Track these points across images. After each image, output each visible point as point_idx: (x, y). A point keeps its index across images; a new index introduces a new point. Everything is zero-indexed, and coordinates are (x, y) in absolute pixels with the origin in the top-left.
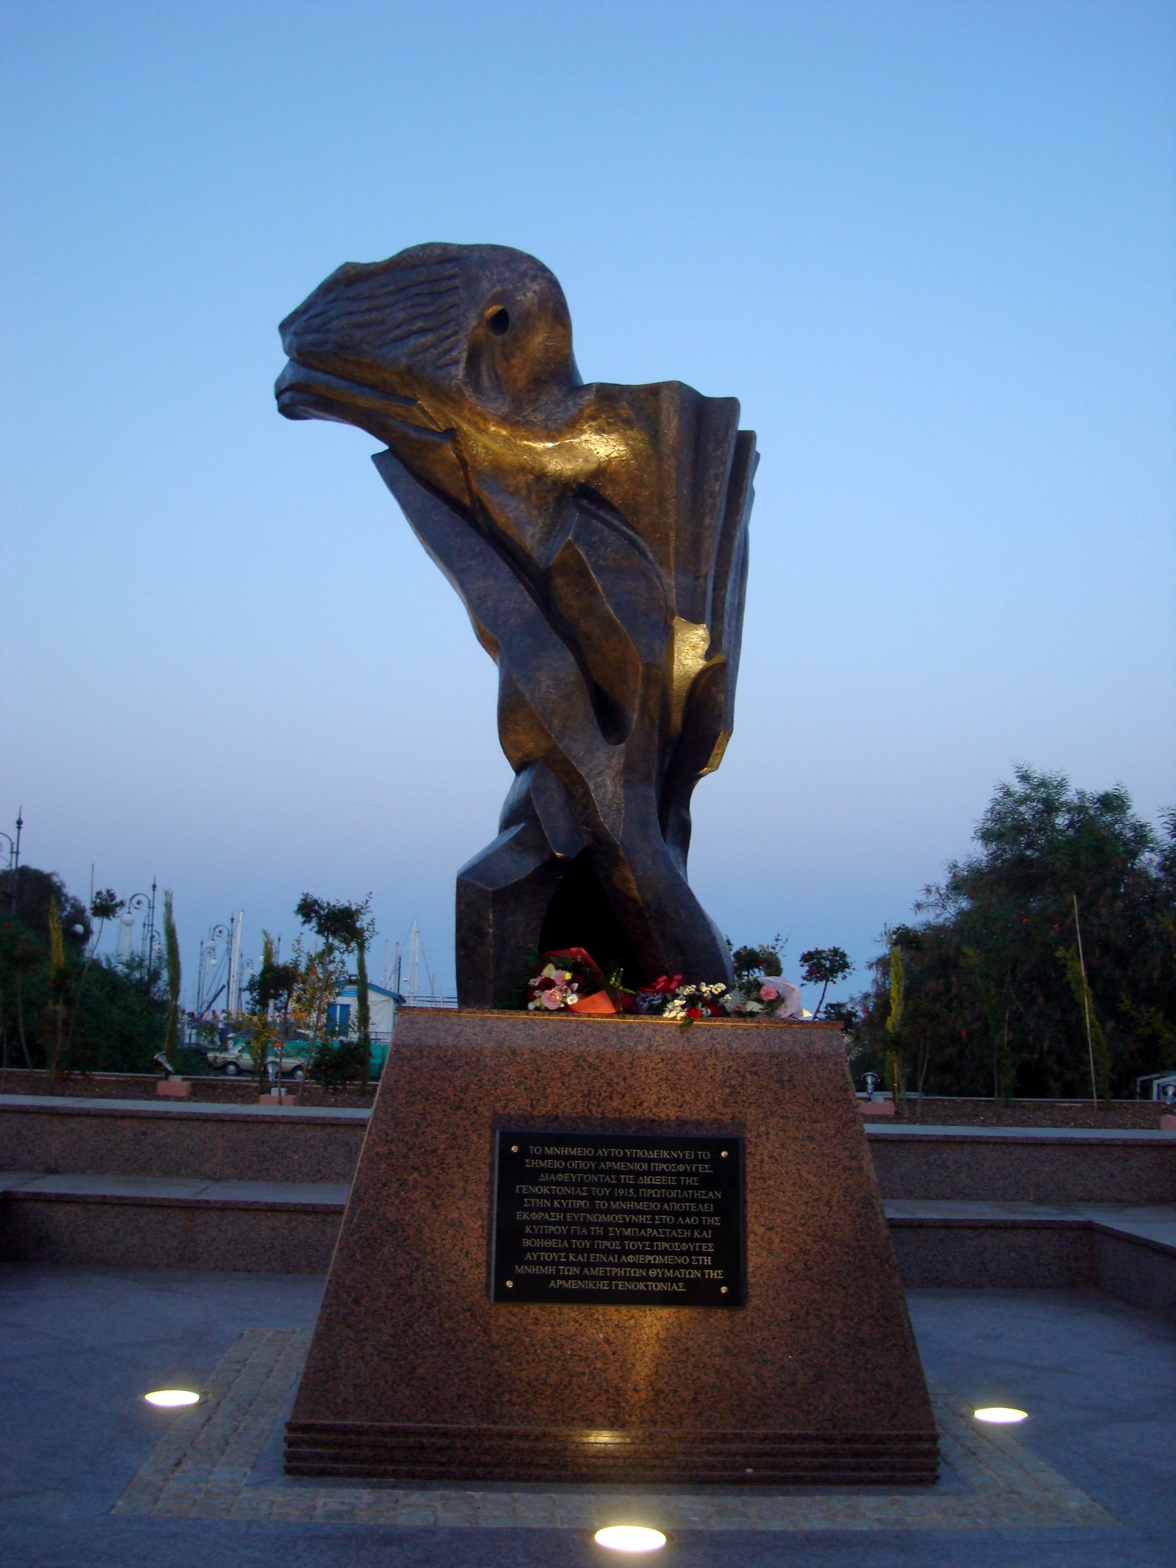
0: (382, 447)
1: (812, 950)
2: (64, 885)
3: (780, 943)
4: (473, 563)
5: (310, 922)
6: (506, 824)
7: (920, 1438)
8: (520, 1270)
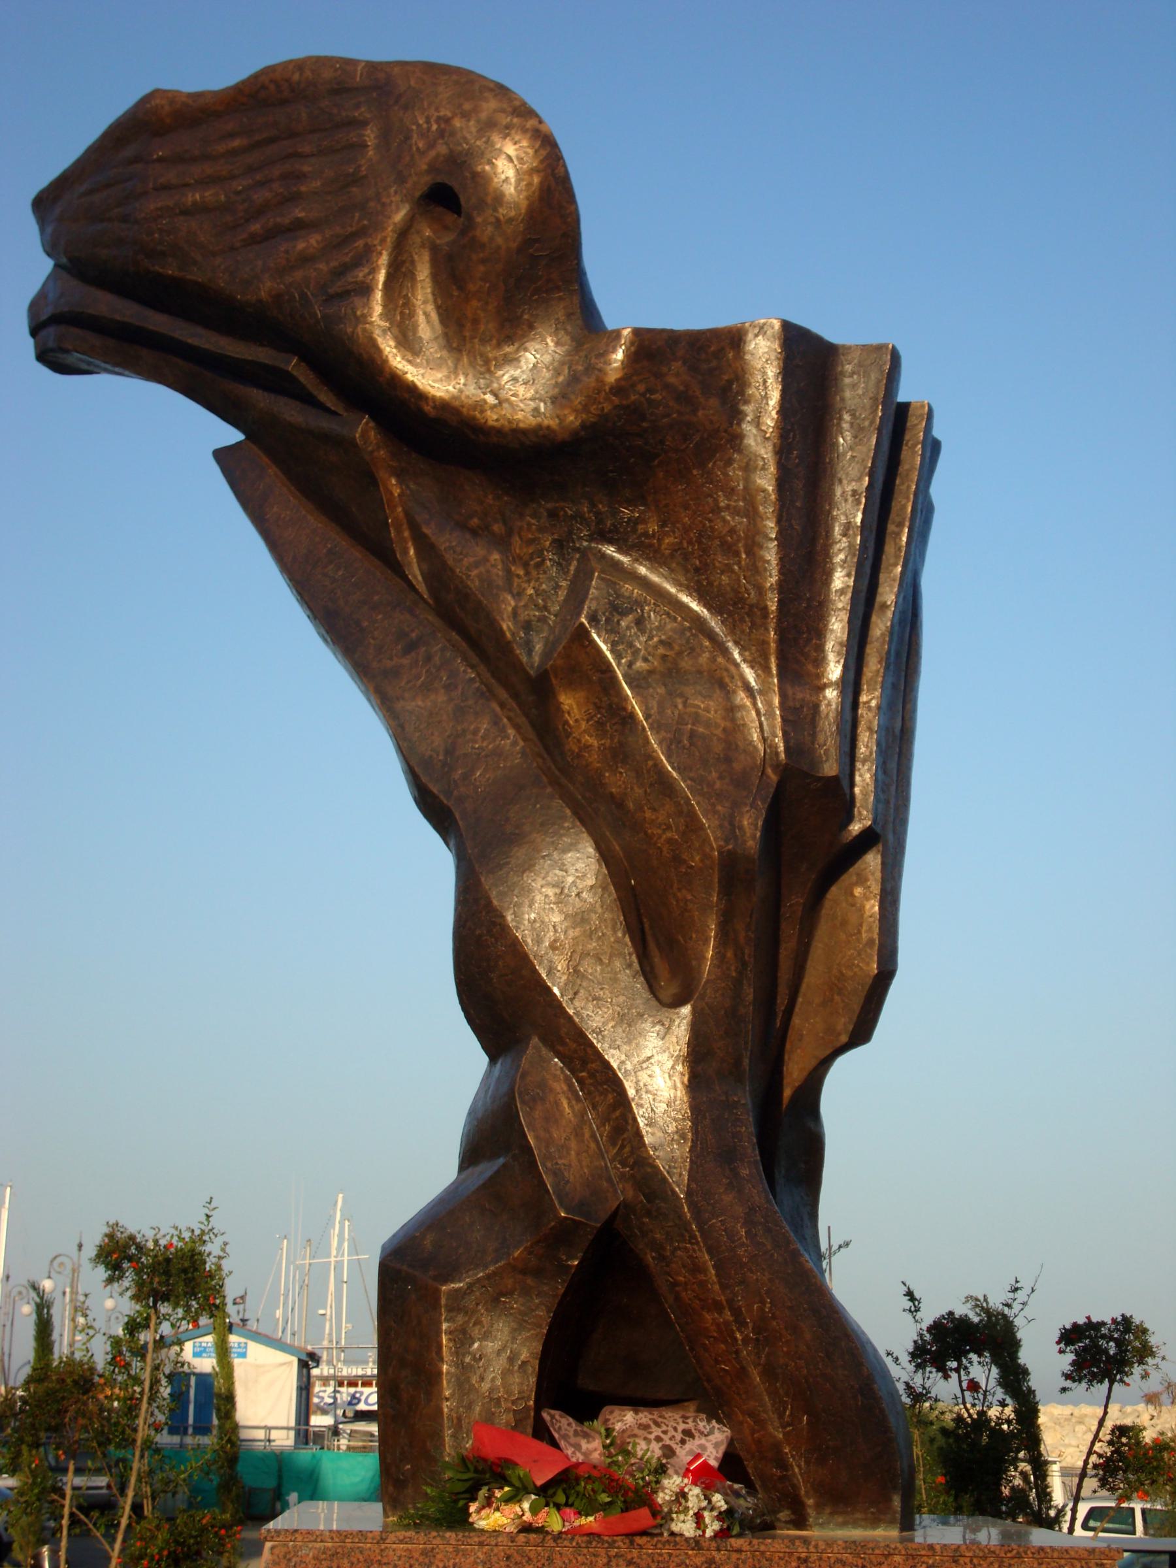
0: (234, 436)
1: (1081, 1321)
3: (1021, 1296)
4: (405, 661)
5: (120, 1278)
6: (471, 1155)
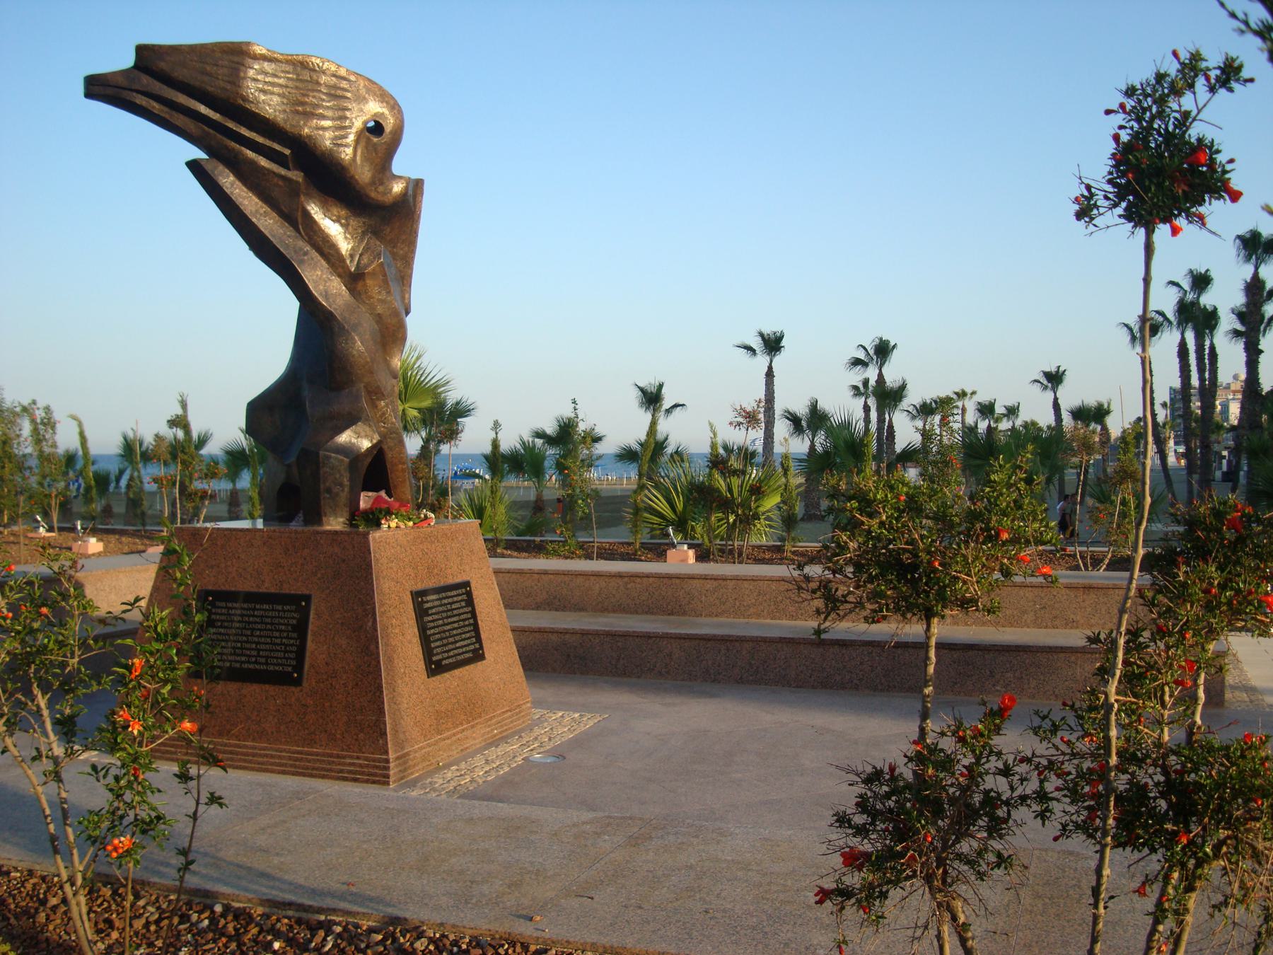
0: (198, 154)
8: (434, 659)
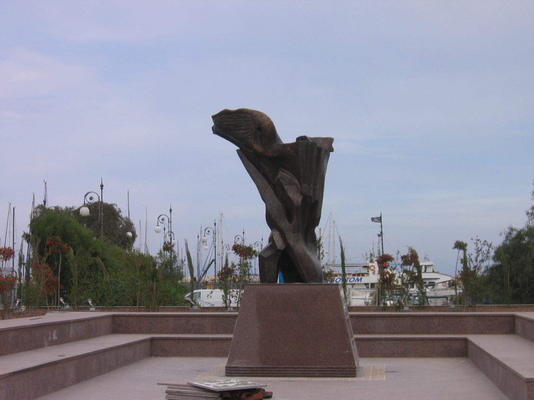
0: (238, 148)
2: (120, 211)
7: (352, 368)
